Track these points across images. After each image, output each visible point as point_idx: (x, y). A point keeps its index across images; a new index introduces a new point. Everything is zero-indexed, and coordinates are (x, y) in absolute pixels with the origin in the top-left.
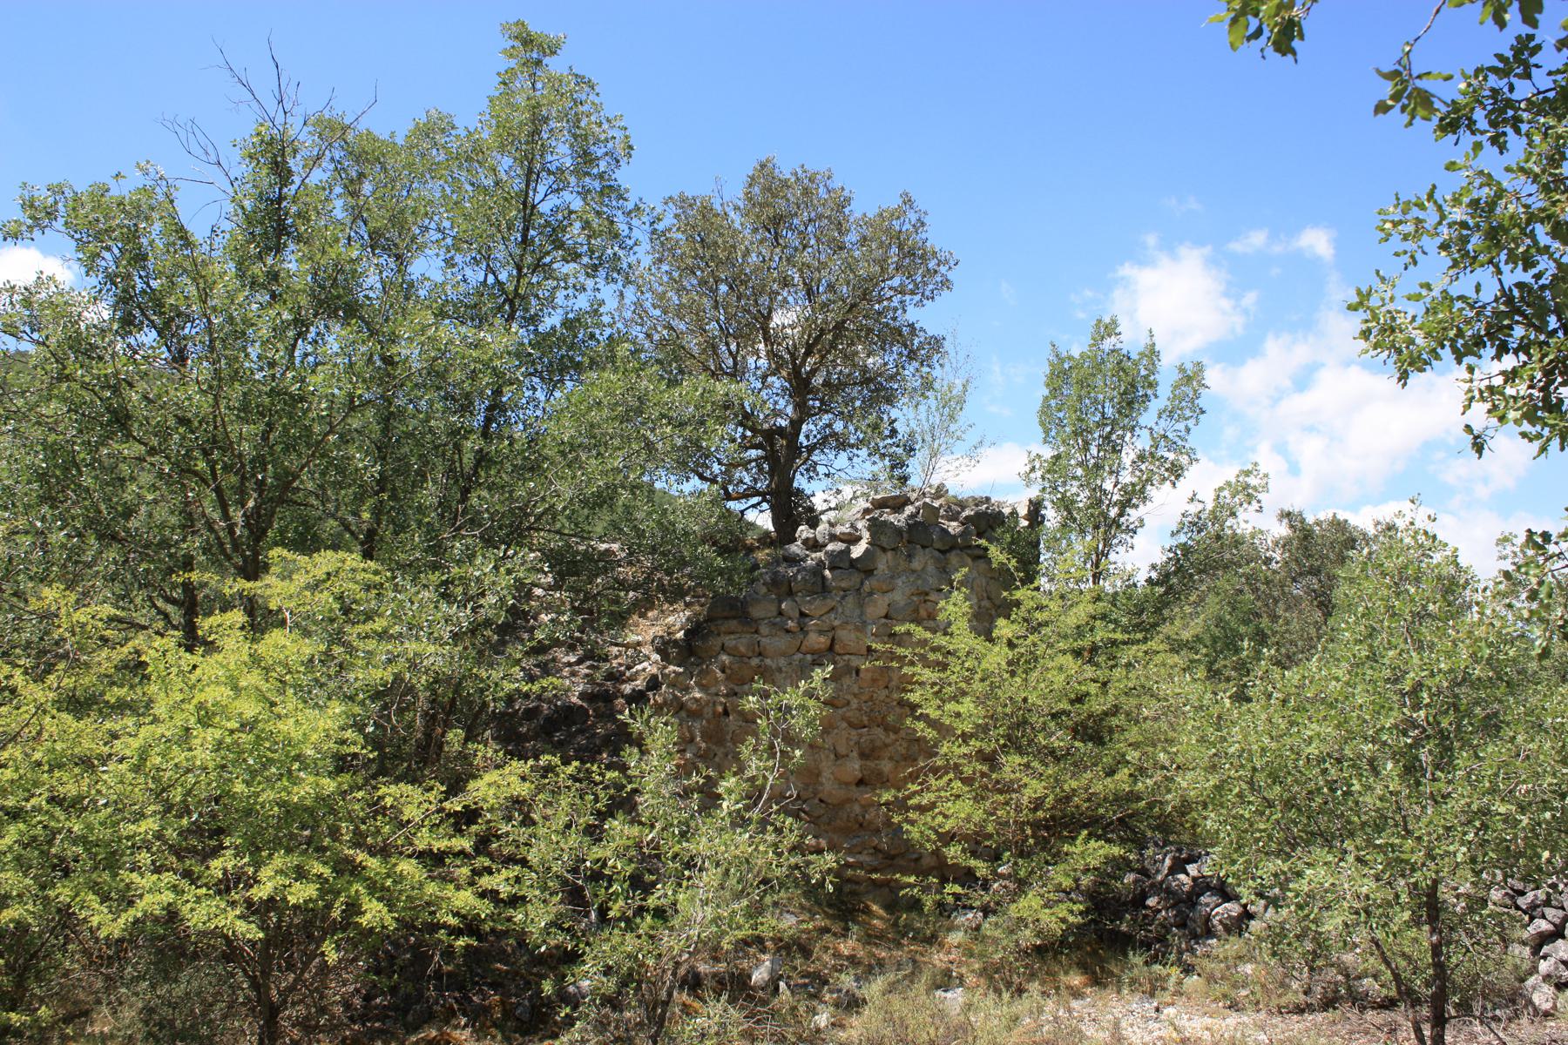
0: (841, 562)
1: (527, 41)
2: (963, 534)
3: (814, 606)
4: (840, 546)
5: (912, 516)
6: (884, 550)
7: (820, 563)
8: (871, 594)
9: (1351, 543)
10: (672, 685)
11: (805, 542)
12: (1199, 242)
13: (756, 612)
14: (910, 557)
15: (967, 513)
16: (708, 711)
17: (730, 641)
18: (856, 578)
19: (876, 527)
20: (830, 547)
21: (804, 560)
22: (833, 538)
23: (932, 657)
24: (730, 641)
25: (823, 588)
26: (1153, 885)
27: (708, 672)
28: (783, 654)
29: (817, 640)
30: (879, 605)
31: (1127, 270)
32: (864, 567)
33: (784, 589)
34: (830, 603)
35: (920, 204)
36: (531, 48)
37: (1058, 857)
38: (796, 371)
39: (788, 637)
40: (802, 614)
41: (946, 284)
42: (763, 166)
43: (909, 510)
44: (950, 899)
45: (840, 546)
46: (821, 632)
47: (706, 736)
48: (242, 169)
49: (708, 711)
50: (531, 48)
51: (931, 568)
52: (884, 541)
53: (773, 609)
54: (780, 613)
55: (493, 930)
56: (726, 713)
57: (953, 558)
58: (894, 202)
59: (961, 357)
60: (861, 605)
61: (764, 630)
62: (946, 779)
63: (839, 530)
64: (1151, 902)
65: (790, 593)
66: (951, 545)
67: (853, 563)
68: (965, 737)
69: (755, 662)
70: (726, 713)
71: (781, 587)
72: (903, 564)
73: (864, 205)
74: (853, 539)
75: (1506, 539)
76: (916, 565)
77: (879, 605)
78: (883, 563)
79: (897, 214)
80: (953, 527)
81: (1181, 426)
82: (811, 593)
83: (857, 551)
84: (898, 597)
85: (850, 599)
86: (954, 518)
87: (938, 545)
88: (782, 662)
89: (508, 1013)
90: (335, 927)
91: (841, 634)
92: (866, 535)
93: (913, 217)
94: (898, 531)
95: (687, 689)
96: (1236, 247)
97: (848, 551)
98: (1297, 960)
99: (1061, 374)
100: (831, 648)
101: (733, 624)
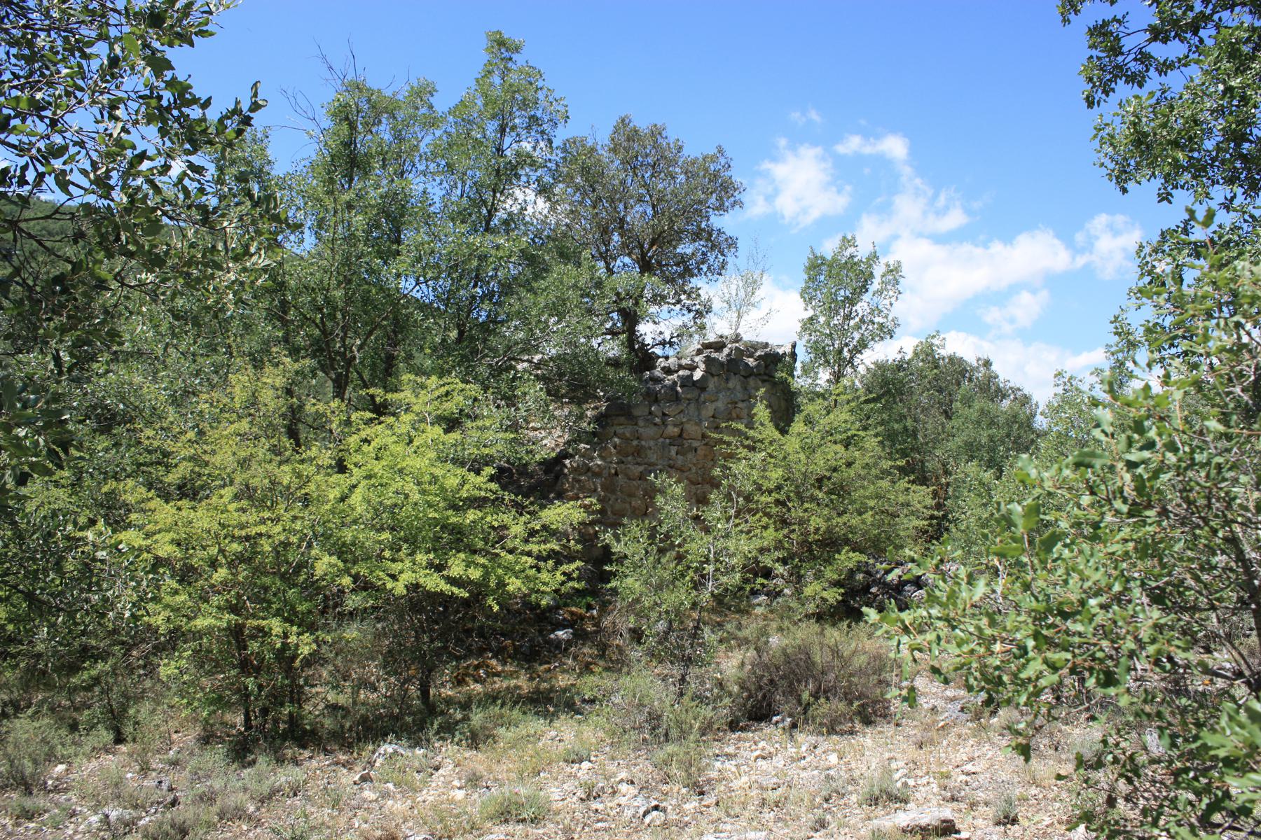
0: (687, 382)
1: (501, 43)
2: (757, 366)
3: (670, 409)
4: (687, 373)
5: (729, 355)
6: (713, 375)
7: (675, 383)
8: (704, 402)
9: (963, 372)
10: (582, 456)
11: (663, 369)
12: (814, 144)
13: (636, 412)
14: (727, 380)
15: (758, 353)
16: (605, 473)
17: (620, 430)
18: (696, 392)
19: (709, 361)
20: (681, 373)
21: (663, 380)
22: (681, 367)
23: (746, 443)
24: (620, 430)
25: (676, 398)
26: (874, 581)
27: (606, 448)
28: (653, 439)
29: (673, 430)
30: (709, 409)
31: (766, 165)
32: (701, 386)
33: (653, 398)
34: (681, 407)
35: (729, 154)
36: (502, 46)
37: (829, 561)
38: (643, 255)
39: (655, 428)
40: (664, 414)
41: (739, 203)
42: (623, 120)
43: (726, 351)
44: (759, 587)
45: (687, 373)
46: (675, 425)
47: (604, 488)
48: (327, 123)
49: (605, 473)
50: (502, 46)
51: (738, 387)
52: (713, 370)
53: (647, 411)
54: (650, 413)
55: (33, 621)
56: (616, 474)
57: (752, 381)
58: (712, 151)
59: (760, 256)
60: (698, 409)
61: (641, 423)
62: (758, 516)
63: (684, 362)
64: (874, 590)
65: (656, 401)
66: (749, 373)
67: (695, 383)
68: (770, 492)
69: (635, 443)
70: (616, 474)
71: (652, 397)
72: (723, 384)
73: (693, 151)
74: (693, 368)
75: (1060, 374)
76: (731, 385)
77: (709, 409)
78: (712, 384)
79: (714, 159)
80: (751, 362)
81: (887, 302)
82: (669, 401)
83: (697, 375)
84: (720, 405)
85: (692, 405)
86: (751, 356)
87: (743, 373)
88: (652, 443)
89: (516, 649)
90: (494, 592)
91: (687, 426)
92: (702, 366)
93: (723, 161)
94: (722, 364)
95: (592, 459)
96: (841, 149)
97: (692, 376)
98: (314, 690)
99: (816, 266)
100: (680, 436)
101: (622, 419)
